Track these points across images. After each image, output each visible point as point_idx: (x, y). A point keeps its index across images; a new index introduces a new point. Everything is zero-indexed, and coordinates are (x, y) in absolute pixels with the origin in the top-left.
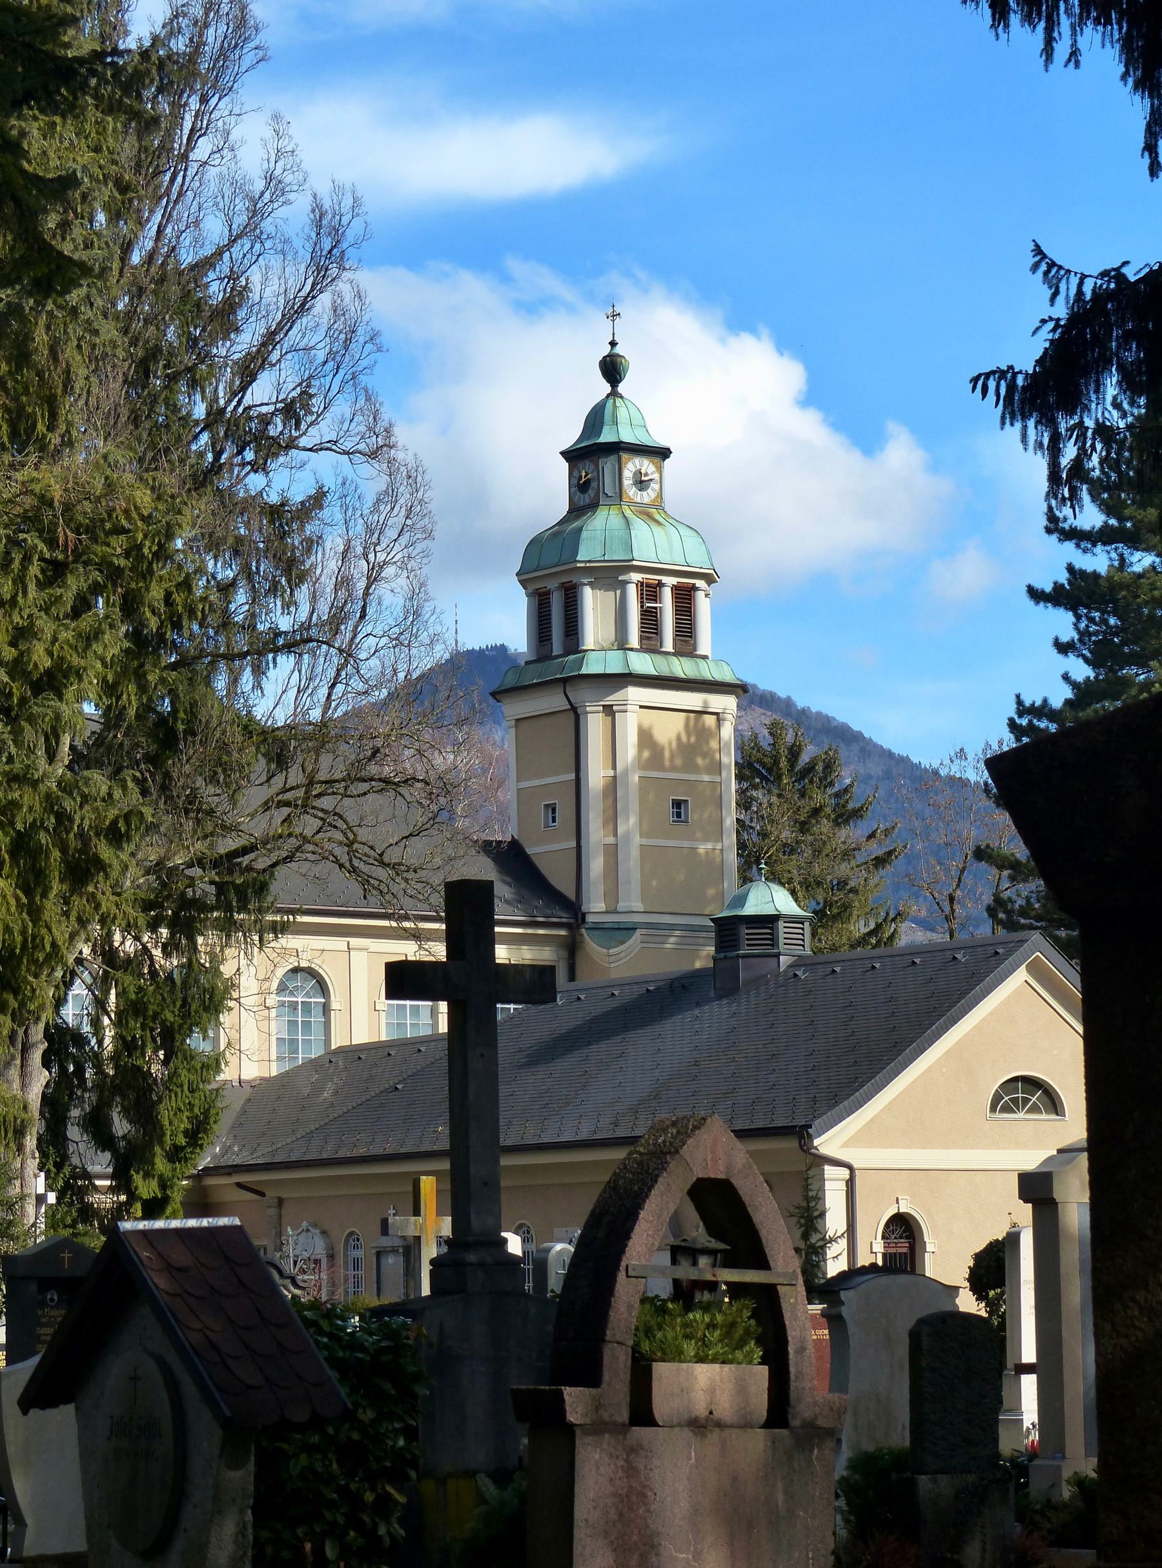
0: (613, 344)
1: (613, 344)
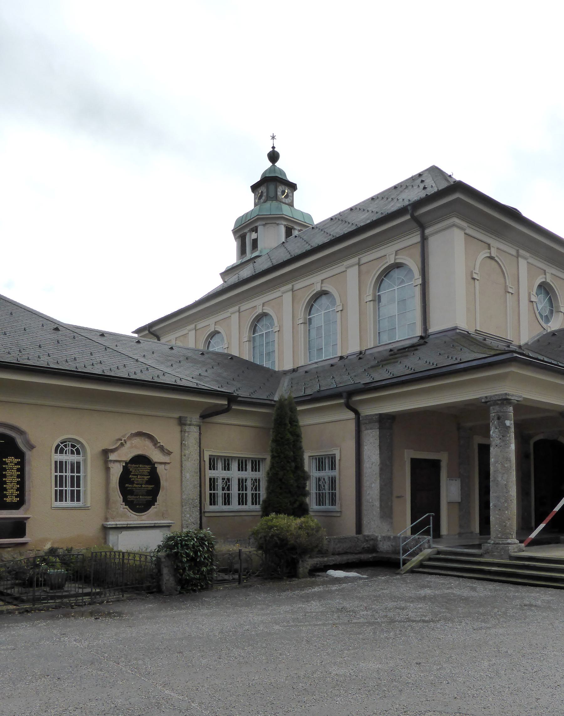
0: (273, 156)
1: (273, 156)
